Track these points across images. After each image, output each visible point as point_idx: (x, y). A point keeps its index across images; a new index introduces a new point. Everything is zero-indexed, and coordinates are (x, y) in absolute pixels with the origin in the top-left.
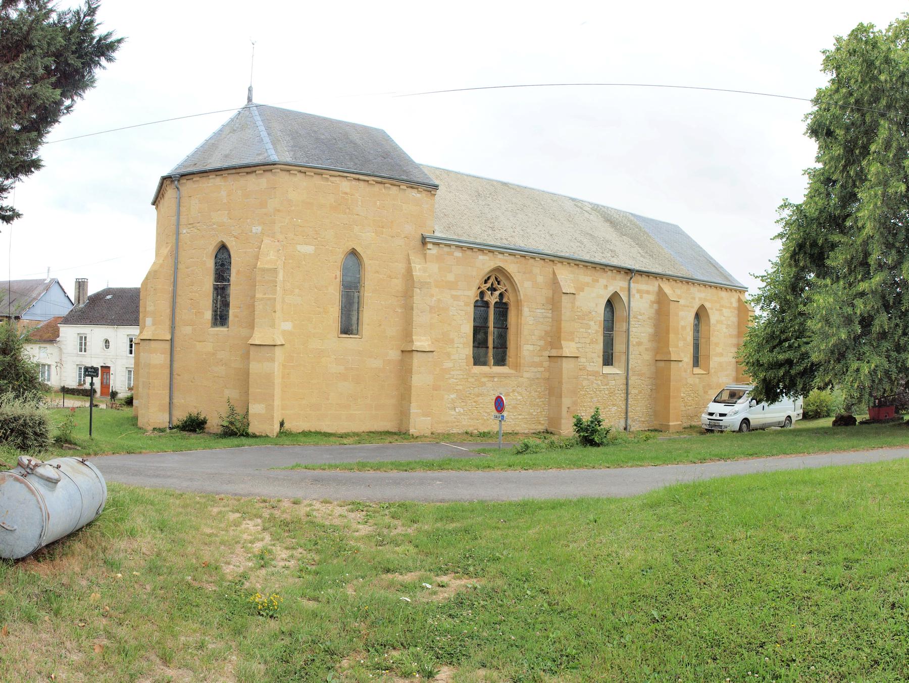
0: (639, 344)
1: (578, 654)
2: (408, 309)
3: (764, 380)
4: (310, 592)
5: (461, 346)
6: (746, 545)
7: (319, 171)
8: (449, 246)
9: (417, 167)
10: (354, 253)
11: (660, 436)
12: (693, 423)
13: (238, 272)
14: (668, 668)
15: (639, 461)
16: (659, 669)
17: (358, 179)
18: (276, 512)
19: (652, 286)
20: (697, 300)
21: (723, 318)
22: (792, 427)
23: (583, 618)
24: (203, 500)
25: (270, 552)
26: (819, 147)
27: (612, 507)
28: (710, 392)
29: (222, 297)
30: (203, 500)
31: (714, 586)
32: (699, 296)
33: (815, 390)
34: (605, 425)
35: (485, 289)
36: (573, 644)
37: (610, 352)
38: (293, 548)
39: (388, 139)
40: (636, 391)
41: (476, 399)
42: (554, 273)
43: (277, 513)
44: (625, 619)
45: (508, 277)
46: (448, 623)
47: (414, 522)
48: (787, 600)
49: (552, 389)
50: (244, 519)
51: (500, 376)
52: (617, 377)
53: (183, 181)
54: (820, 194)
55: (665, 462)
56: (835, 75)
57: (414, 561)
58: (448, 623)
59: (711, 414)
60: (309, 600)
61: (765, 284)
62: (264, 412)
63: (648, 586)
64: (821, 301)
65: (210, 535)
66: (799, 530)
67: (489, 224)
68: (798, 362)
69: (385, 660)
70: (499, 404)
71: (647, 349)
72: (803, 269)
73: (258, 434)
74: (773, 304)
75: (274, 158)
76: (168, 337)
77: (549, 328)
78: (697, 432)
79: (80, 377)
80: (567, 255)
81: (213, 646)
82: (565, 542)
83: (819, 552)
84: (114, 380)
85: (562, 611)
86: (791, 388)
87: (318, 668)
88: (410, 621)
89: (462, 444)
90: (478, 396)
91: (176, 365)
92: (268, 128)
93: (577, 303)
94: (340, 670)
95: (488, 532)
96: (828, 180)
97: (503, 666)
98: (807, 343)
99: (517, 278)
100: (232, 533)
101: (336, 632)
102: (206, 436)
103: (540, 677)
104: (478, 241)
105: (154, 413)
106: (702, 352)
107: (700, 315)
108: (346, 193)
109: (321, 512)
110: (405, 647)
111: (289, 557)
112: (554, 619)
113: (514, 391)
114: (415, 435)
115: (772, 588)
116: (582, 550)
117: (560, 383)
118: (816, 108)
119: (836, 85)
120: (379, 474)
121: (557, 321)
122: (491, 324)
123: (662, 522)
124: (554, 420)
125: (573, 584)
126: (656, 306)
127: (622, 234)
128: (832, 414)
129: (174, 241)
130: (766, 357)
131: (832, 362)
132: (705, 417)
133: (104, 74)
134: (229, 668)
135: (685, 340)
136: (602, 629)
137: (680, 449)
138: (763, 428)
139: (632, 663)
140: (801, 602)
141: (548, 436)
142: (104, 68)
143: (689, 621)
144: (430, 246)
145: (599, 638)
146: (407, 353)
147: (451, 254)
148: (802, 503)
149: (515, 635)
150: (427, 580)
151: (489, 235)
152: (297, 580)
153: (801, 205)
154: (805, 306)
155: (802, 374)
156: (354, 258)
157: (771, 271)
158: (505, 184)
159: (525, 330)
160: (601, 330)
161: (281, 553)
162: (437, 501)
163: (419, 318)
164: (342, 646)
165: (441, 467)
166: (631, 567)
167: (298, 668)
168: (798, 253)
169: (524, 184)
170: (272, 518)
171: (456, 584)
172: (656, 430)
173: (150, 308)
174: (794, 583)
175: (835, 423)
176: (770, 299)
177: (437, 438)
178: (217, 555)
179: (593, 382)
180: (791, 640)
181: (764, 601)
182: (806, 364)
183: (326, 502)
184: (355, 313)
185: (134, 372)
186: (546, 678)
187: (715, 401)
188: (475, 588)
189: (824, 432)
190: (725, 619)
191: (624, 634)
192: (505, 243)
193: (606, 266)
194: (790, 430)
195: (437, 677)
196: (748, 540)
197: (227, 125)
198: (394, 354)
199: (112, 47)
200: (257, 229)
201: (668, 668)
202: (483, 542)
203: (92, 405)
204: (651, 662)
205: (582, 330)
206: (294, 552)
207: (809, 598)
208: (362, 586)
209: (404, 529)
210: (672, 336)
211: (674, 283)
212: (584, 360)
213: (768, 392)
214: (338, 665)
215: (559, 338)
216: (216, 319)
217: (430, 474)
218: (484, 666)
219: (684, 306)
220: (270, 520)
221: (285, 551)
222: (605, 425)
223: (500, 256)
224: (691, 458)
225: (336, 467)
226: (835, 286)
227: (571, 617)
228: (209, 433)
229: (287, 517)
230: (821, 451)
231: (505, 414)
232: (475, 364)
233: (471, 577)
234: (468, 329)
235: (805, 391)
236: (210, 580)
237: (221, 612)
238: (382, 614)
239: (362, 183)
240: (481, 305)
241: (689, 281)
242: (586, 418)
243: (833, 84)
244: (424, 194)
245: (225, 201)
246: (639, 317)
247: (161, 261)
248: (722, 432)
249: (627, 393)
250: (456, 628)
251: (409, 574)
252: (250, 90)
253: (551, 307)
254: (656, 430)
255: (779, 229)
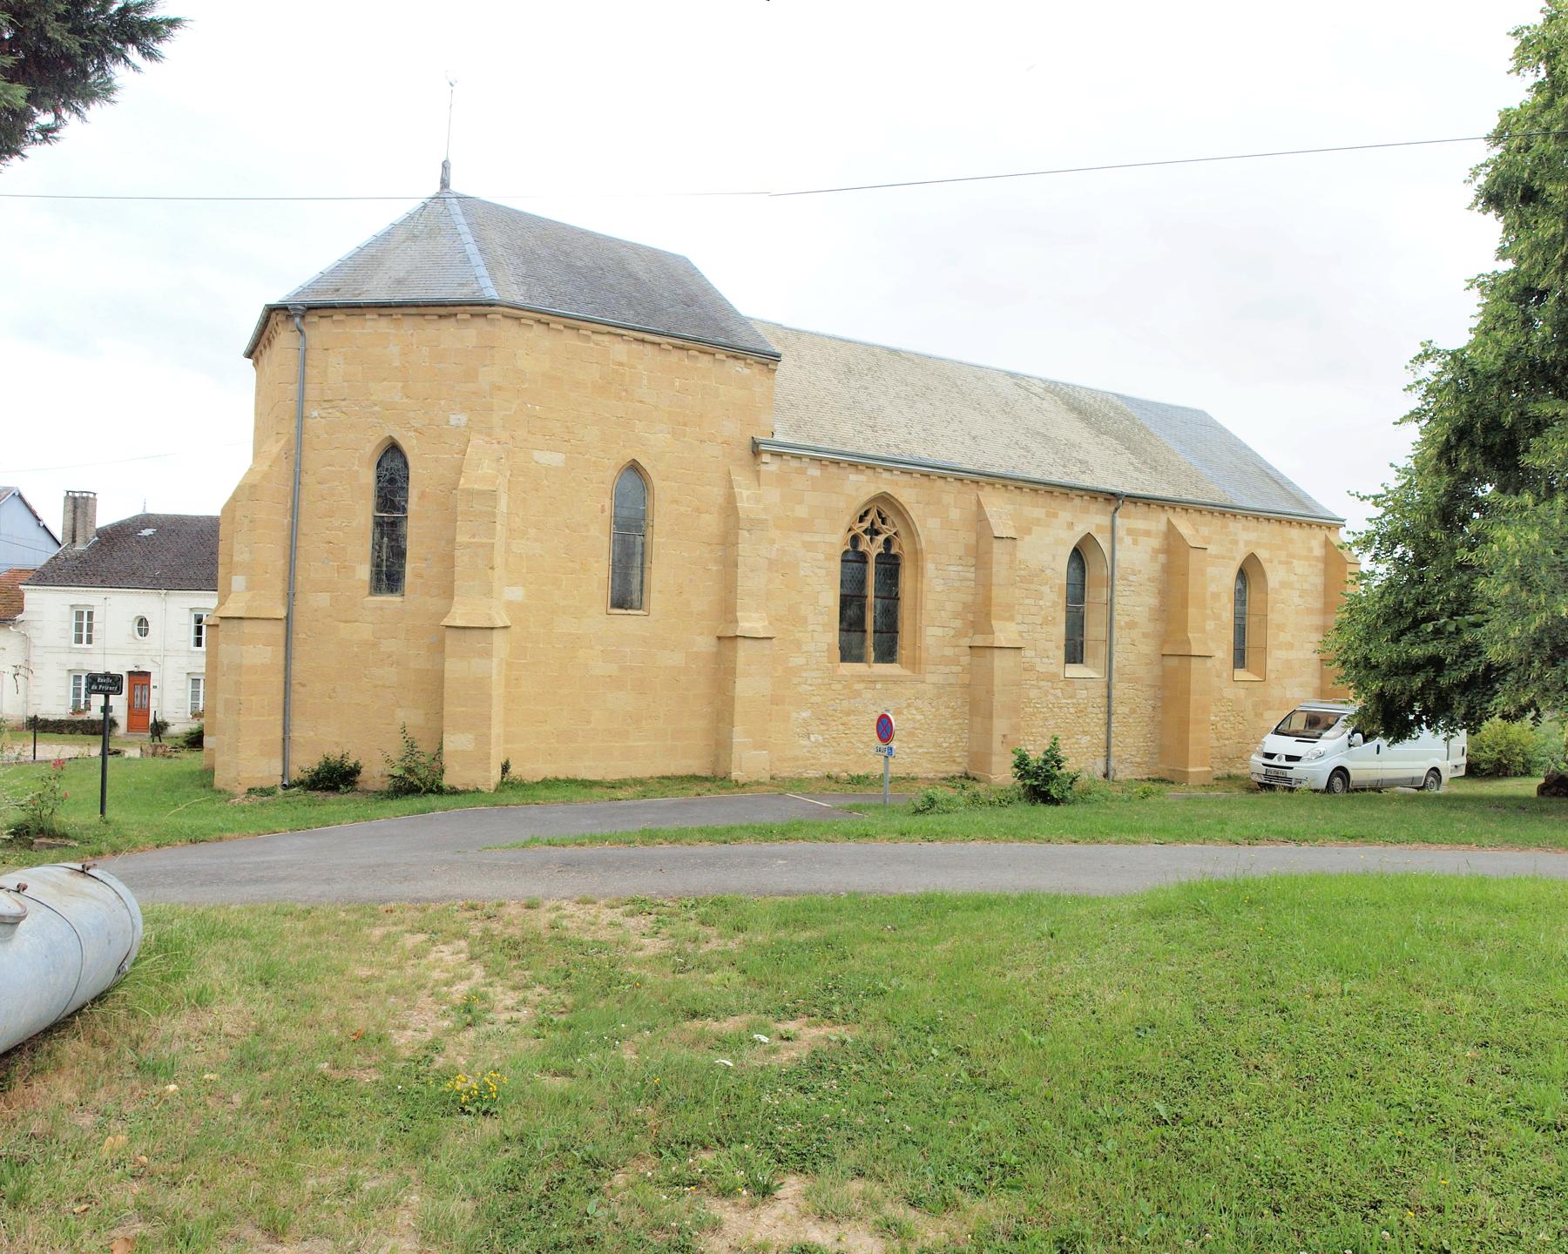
0: (1131, 625)
1: (1021, 1164)
2: (729, 566)
3: (1380, 696)
4: (557, 1062)
5: (819, 628)
6: (1342, 1008)
7: (574, 323)
8: (799, 457)
9: (744, 322)
10: (634, 468)
11: (1170, 792)
12: (1234, 771)
13: (423, 495)
14: (1185, 1209)
15: (1132, 833)
16: (1167, 1209)
17: (643, 341)
18: (494, 925)
19: (1156, 522)
20: (1242, 545)
21: (1295, 578)
22: (1442, 790)
23: (1029, 1102)
24: (352, 917)
25: (484, 998)
26: (1506, 228)
27: (1082, 912)
28: (1267, 715)
29: (390, 539)
30: (352, 917)
31: (1276, 1075)
32: (1245, 538)
33: (1497, 719)
34: (1069, 767)
35: (860, 531)
36: (1012, 1145)
37: (1079, 639)
38: (526, 987)
39: (693, 272)
40: (1127, 710)
41: (845, 719)
42: (979, 503)
43: (496, 927)
44: (1106, 1111)
45: (901, 512)
46: (797, 1102)
47: (739, 929)
48: (1431, 1129)
49: (976, 702)
50: (434, 943)
51: (885, 679)
52: (1090, 684)
53: (312, 318)
54: (1506, 323)
55: (1179, 839)
56: (1543, 73)
57: (740, 996)
58: (797, 1102)
59: (1270, 756)
60: (555, 1075)
61: (1381, 511)
62: (471, 747)
63: (1149, 1058)
64: (1510, 539)
65: (366, 981)
66: (1459, 996)
67: (866, 421)
68: (1455, 663)
69: (689, 1168)
70: (885, 729)
71: (1145, 635)
72: (1467, 477)
73: (460, 788)
74: (1399, 550)
75: (491, 293)
76: (281, 612)
77: (970, 599)
78: (1242, 787)
79: (77, 694)
80: (1002, 471)
81: (374, 1184)
82: (998, 969)
83: (1505, 1049)
84: (160, 700)
85: (993, 1088)
86: (1439, 712)
87: (572, 1193)
88: (733, 1099)
89: (821, 797)
90: (848, 714)
91: (297, 666)
92: (478, 239)
93: (1020, 555)
94: (610, 1193)
95: (865, 947)
96: (1528, 291)
97: (892, 1176)
98: (1477, 625)
99: (915, 513)
100: (410, 971)
101: (603, 1126)
102: (358, 797)
103: (954, 1197)
104: (848, 449)
105: (247, 758)
106: (1251, 640)
107: (1248, 573)
108: (621, 364)
109: (575, 919)
110: (723, 1145)
111: (518, 1003)
112: (979, 1100)
113: (909, 706)
114: (741, 781)
115: (1397, 1100)
116: (1028, 983)
117: (990, 692)
118: (1498, 151)
119: (1547, 94)
120: (678, 849)
121: (984, 586)
122: (870, 591)
123: (1173, 946)
124: (980, 757)
125: (1013, 1041)
126: (1162, 558)
127: (1100, 432)
128: (1537, 771)
129: (293, 431)
130: (1384, 652)
131: (1537, 664)
132: (1257, 761)
133: (129, 76)
134: (405, 1218)
135: (1217, 618)
136: (1064, 1124)
137: (1207, 817)
138: (1377, 788)
139: (1118, 1191)
140: (1464, 1141)
141: (968, 783)
142: (135, 68)
143: (1225, 1131)
144: (766, 458)
145: (1059, 1140)
146: (728, 640)
147: (802, 472)
148: (1465, 943)
149: (912, 1124)
150: (762, 1028)
151: (866, 440)
152: (532, 1043)
153: (1462, 351)
154: (1471, 550)
155: (1466, 686)
156: (634, 476)
157: (1394, 485)
158: (894, 352)
159: (929, 603)
160: (1062, 601)
161: (504, 997)
162: (779, 894)
163: (750, 581)
164: (613, 1150)
165: (785, 836)
166: (1116, 1020)
167: (535, 1197)
168: (1457, 447)
169: (927, 352)
170: (487, 936)
171: (810, 1035)
172: (1162, 780)
173: (241, 555)
174: (1446, 1099)
175: (1542, 790)
176: (1392, 540)
177: (780, 785)
178: (380, 1015)
179: (1046, 693)
180: (1440, 1210)
181: (1380, 1122)
182: (1473, 666)
183: (585, 902)
184: (637, 572)
185: (206, 682)
186: (965, 1201)
187: (1277, 732)
188: (844, 1042)
189: (1519, 805)
190: (1299, 1140)
191: (1104, 1139)
192: (894, 453)
193: (1072, 488)
194: (1439, 797)
195: (779, 1193)
196: (1346, 998)
197: (401, 224)
198: (704, 643)
199: (155, 30)
200: (459, 419)
201: (1185, 1209)
202: (856, 964)
203: (105, 752)
204: (1153, 1194)
205: (1028, 601)
206: (528, 994)
207: (1481, 1137)
208: (650, 1044)
209: (722, 942)
210: (1192, 611)
211: (1196, 516)
212: (1033, 653)
213: (1390, 719)
214: (607, 1184)
215: (988, 615)
216: (379, 580)
217: (766, 847)
218: (861, 1174)
219: (1217, 557)
220: (482, 941)
221: (511, 993)
222: (1069, 767)
223: (886, 475)
224: (1229, 834)
225: (604, 839)
226: (1543, 508)
227: (1009, 1099)
228: (365, 792)
229: (516, 933)
230: (1508, 843)
231: (894, 744)
232: (843, 659)
233: (836, 1023)
234: (830, 599)
235: (1473, 721)
236: (367, 1062)
237: (388, 1120)
238: (685, 1090)
239: (649, 347)
240: (854, 558)
241: (1225, 511)
242: (1036, 755)
243: (1539, 92)
244: (756, 369)
245: (397, 364)
246: (1131, 578)
247: (265, 468)
248: (1291, 789)
249: (1109, 713)
250: (812, 1110)
251: (731, 1020)
252: (445, 166)
253: (973, 561)
254: (1162, 780)
255: (1414, 402)
